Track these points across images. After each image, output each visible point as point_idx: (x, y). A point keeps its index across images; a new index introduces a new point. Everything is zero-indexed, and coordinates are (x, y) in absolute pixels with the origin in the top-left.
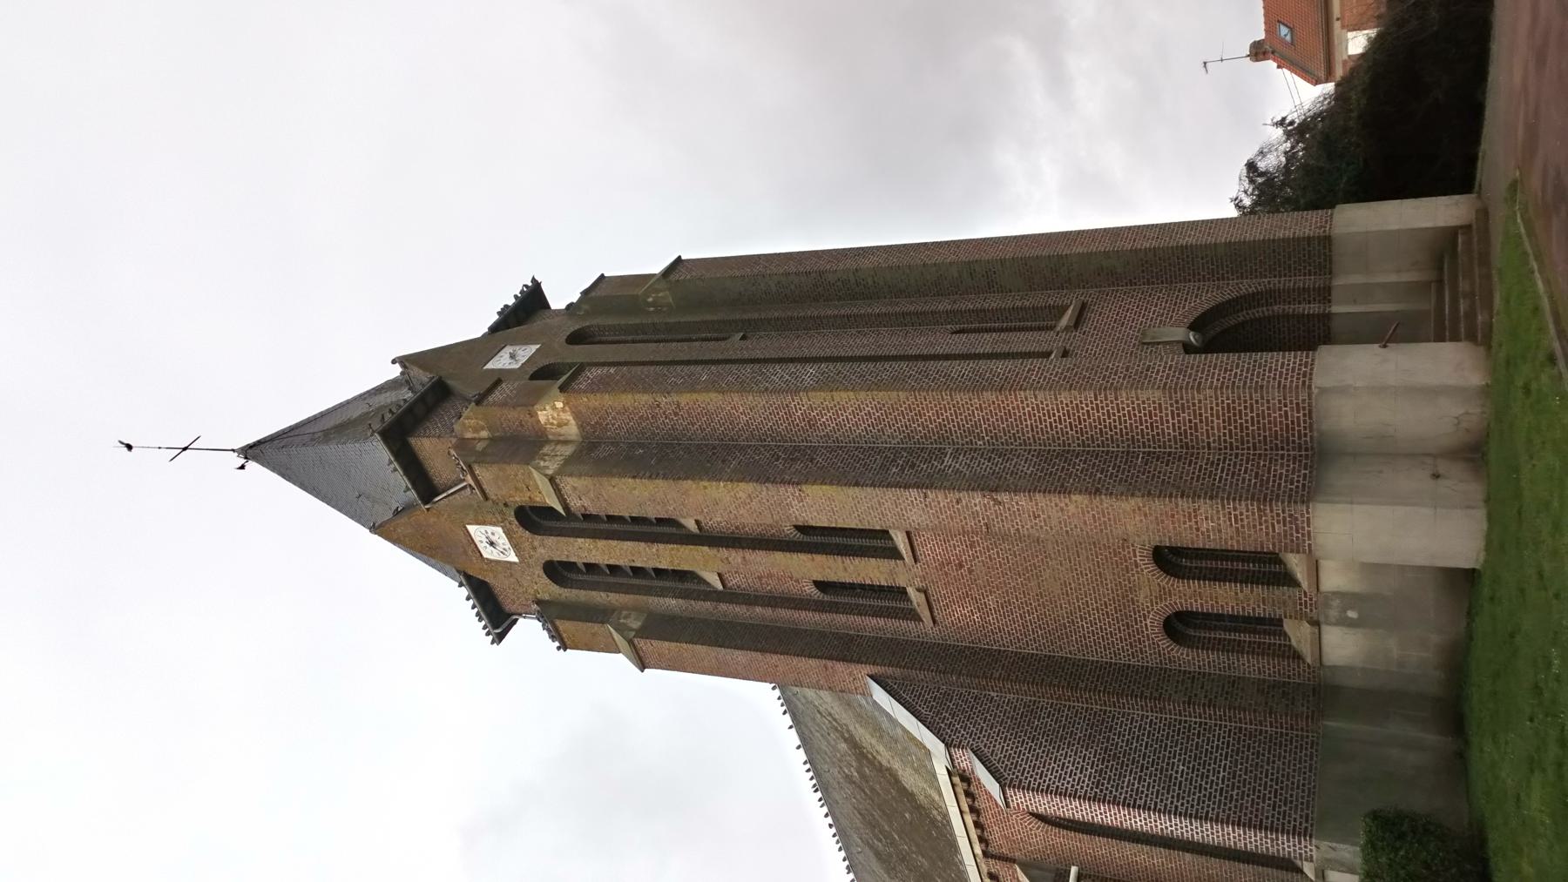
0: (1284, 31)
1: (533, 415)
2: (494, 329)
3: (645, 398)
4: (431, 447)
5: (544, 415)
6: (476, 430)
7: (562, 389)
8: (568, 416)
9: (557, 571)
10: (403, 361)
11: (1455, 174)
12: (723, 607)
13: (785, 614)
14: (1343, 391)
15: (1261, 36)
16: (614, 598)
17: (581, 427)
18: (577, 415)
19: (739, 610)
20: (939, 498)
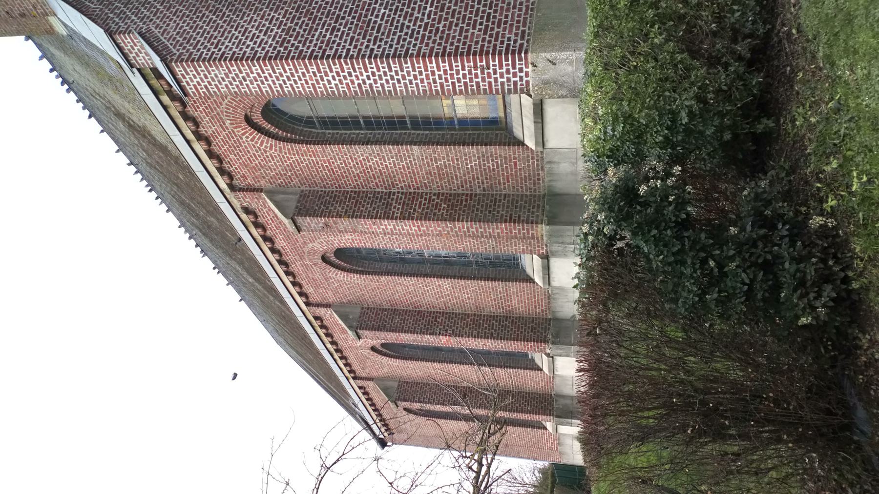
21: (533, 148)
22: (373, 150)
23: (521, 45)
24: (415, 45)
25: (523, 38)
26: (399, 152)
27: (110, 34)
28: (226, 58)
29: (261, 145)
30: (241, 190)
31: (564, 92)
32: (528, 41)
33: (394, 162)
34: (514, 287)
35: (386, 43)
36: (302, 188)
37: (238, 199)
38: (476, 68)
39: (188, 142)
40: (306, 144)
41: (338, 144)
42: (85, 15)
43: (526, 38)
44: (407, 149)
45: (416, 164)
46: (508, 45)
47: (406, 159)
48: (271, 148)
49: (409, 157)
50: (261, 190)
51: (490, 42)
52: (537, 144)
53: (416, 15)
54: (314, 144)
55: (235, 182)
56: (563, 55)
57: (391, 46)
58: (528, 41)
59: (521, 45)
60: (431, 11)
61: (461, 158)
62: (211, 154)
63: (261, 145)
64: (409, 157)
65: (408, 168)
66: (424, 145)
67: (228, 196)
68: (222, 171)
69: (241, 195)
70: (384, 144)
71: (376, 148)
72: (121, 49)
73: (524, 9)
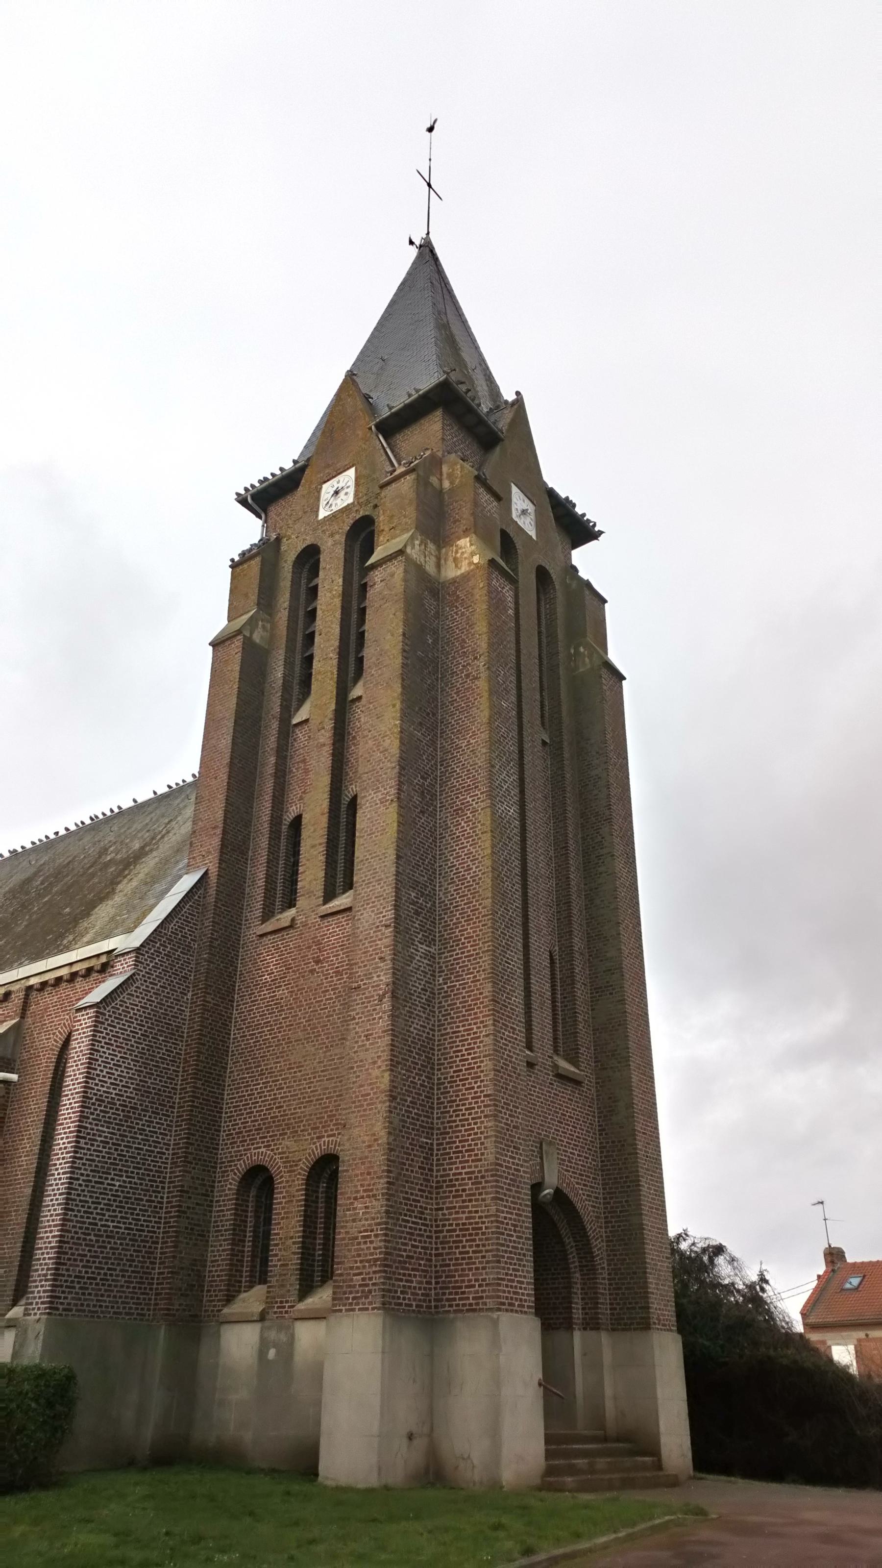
0: (855, 1281)
1: (466, 533)
2: (551, 494)
3: (483, 645)
4: (433, 430)
5: (465, 544)
6: (450, 476)
7: (492, 562)
8: (464, 568)
9: (310, 558)
10: (519, 403)
11: (710, 1457)
12: (275, 725)
13: (269, 785)
14: (495, 1343)
15: (850, 1259)
16: (283, 616)
17: (454, 581)
18: (466, 577)
19: (271, 741)
20: (385, 940)
21: (7, 1316)
22: (35, 1146)
23: (57, 1309)
24: (76, 1216)
25: (64, 1310)
26: (30, 1173)
27: (96, 1005)
28: (93, 1054)
29: (60, 1032)
30: (27, 996)
31: (16, 1347)
32: (61, 1315)
33: (23, 1165)
34: (258, 913)
35: (83, 1191)
36: (18, 1060)
37: (18, 991)
38: (48, 1269)
39: (71, 964)
40: (53, 1078)
41: (47, 1111)
42: (162, 922)
43: (64, 1313)
44: (30, 1182)
45: (17, 1189)
46: (60, 1298)
47: (23, 1179)
48: (55, 1040)
49: (24, 1183)
50: (23, 1016)
51: (66, 1281)
52: (9, 1320)
53: (107, 1214)
54: (51, 1086)
55: (35, 993)
56: (40, 1345)
57: (79, 1195)
58: (61, 1315)
59: (57, 1309)
60: (109, 1226)
61: (14, 1238)
62: (59, 980)
63: (60, 1032)
64: (24, 1183)
65: (15, 1180)
66: (31, 1200)
67: (23, 981)
68: (44, 985)
69: (22, 995)
70: (39, 1158)
71: (36, 1149)
72: (85, 1008)
73: (95, 1309)
